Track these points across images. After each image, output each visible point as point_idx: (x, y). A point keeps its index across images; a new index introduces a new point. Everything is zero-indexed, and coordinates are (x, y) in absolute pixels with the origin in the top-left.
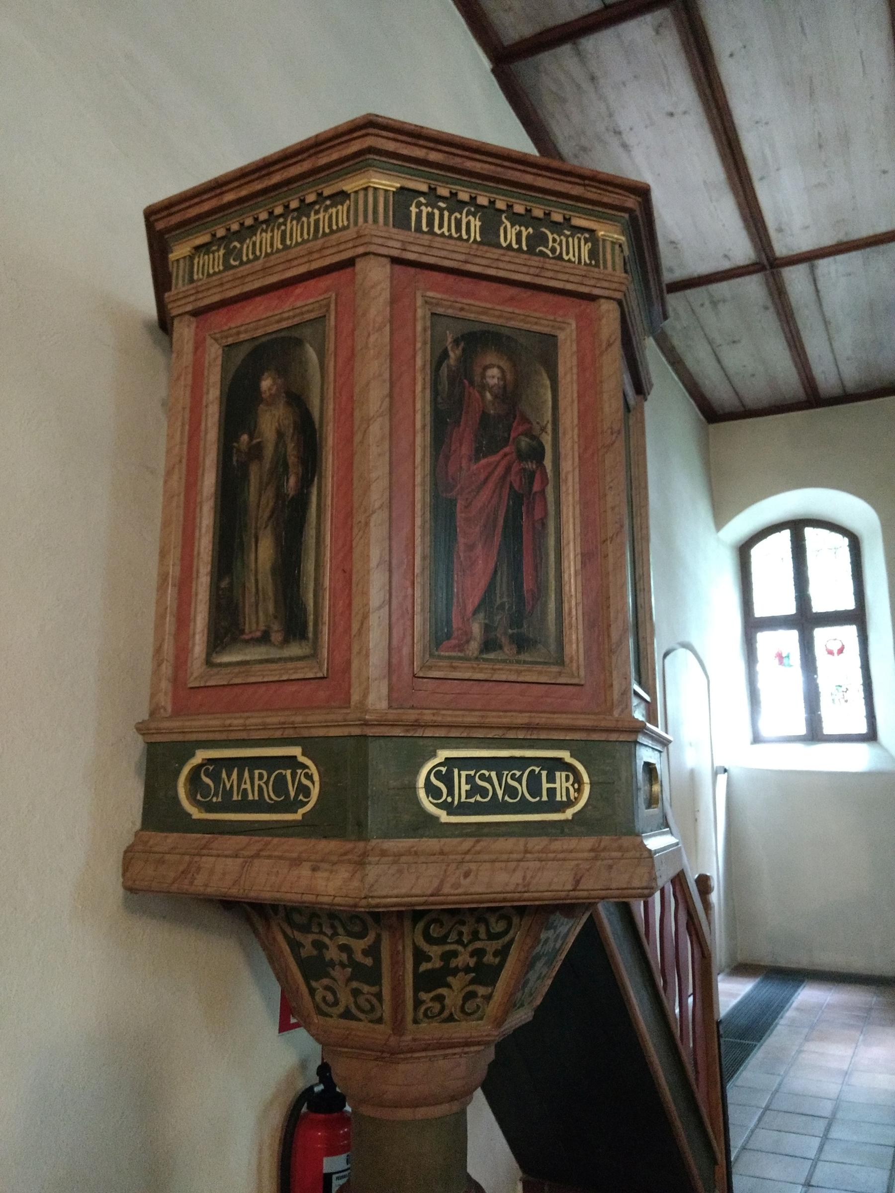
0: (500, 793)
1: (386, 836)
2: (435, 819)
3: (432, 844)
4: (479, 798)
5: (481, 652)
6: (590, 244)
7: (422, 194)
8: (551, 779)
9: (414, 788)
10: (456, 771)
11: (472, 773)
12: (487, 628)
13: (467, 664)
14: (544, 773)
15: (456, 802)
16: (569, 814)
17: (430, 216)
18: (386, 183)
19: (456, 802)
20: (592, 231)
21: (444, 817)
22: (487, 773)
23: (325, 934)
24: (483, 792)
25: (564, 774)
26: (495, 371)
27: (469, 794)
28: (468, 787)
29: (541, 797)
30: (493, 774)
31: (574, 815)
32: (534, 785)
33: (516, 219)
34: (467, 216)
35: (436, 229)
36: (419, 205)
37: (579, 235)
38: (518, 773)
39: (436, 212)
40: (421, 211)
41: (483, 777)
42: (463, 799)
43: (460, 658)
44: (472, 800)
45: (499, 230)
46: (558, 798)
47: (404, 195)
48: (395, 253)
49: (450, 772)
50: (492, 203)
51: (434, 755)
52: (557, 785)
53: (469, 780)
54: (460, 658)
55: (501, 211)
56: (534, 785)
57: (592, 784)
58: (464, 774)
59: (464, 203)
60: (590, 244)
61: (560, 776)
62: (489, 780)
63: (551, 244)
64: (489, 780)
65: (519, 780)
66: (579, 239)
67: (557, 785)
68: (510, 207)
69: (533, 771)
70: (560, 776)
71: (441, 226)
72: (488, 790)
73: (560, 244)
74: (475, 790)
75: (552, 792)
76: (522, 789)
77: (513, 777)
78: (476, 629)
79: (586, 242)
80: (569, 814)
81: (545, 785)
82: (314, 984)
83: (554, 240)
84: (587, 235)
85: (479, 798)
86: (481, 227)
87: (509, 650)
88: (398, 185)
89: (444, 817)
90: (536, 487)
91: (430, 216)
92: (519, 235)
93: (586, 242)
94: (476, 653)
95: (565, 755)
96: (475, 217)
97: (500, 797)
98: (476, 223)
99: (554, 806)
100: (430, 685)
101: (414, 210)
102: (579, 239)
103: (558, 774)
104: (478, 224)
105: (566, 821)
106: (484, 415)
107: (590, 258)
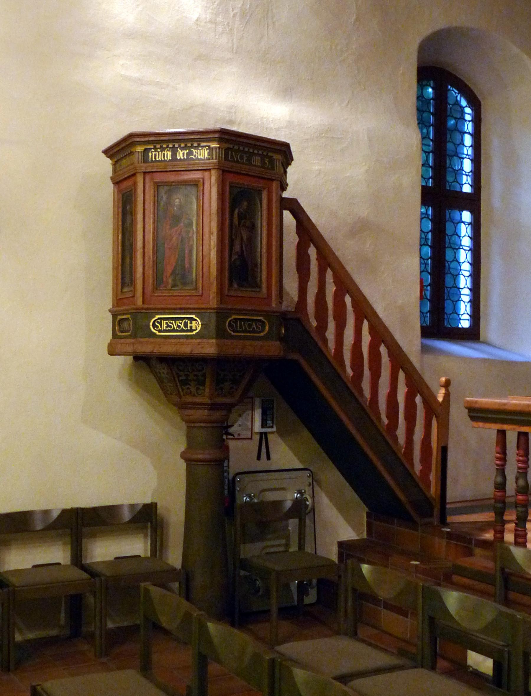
0: (175, 327)
1: (141, 337)
2: (155, 334)
3: (152, 340)
4: (169, 328)
5: (172, 288)
6: (208, 151)
7: (152, 149)
8: (191, 323)
9: (149, 326)
10: (163, 321)
11: (167, 321)
12: (174, 280)
13: (167, 291)
14: (189, 322)
15: (163, 329)
16: (194, 333)
17: (155, 155)
18: (140, 149)
19: (163, 329)
20: (209, 146)
21: (232, 333)
22: (171, 322)
23: (189, 372)
24: (171, 327)
25: (195, 322)
26: (178, 200)
27: (166, 327)
28: (166, 325)
29: (188, 328)
30: (174, 322)
31: (196, 333)
32: (186, 325)
33: (182, 149)
34: (167, 151)
35: (157, 159)
36: (152, 152)
37: (204, 148)
38: (181, 322)
39: (157, 153)
40: (152, 154)
41: (170, 323)
42: (165, 329)
43: (165, 290)
44: (167, 329)
45: (177, 154)
46: (193, 328)
47: (146, 151)
48: (144, 171)
49: (161, 322)
50: (174, 146)
51: (155, 317)
52: (193, 325)
53: (167, 323)
54: (165, 290)
55: (177, 148)
56: (186, 325)
57: (202, 324)
58: (165, 322)
59: (165, 148)
60: (208, 151)
61: (194, 322)
62: (172, 323)
63: (194, 154)
64: (172, 323)
65: (181, 323)
66: (204, 149)
67: (193, 325)
68: (180, 145)
69: (186, 321)
70: (194, 322)
71: (159, 157)
72: (172, 326)
73: (198, 153)
74: (168, 326)
75: (191, 327)
76: (182, 326)
77: (180, 323)
78: (170, 281)
79: (207, 149)
80: (194, 333)
81: (189, 325)
82: (184, 387)
83: (196, 152)
84: (207, 147)
85: (169, 328)
86: (171, 154)
87: (180, 286)
88: (144, 149)
89: (158, 333)
90: (190, 235)
91: (155, 155)
92: (184, 154)
93: (207, 149)
94: (170, 288)
95: (194, 316)
96: (169, 151)
97: (175, 328)
98: (169, 153)
99: (191, 330)
100: (155, 298)
101: (150, 154)
102: (204, 149)
103: (193, 322)
104: (170, 153)
105: (193, 335)
106: (273, 157)
107: (208, 156)
